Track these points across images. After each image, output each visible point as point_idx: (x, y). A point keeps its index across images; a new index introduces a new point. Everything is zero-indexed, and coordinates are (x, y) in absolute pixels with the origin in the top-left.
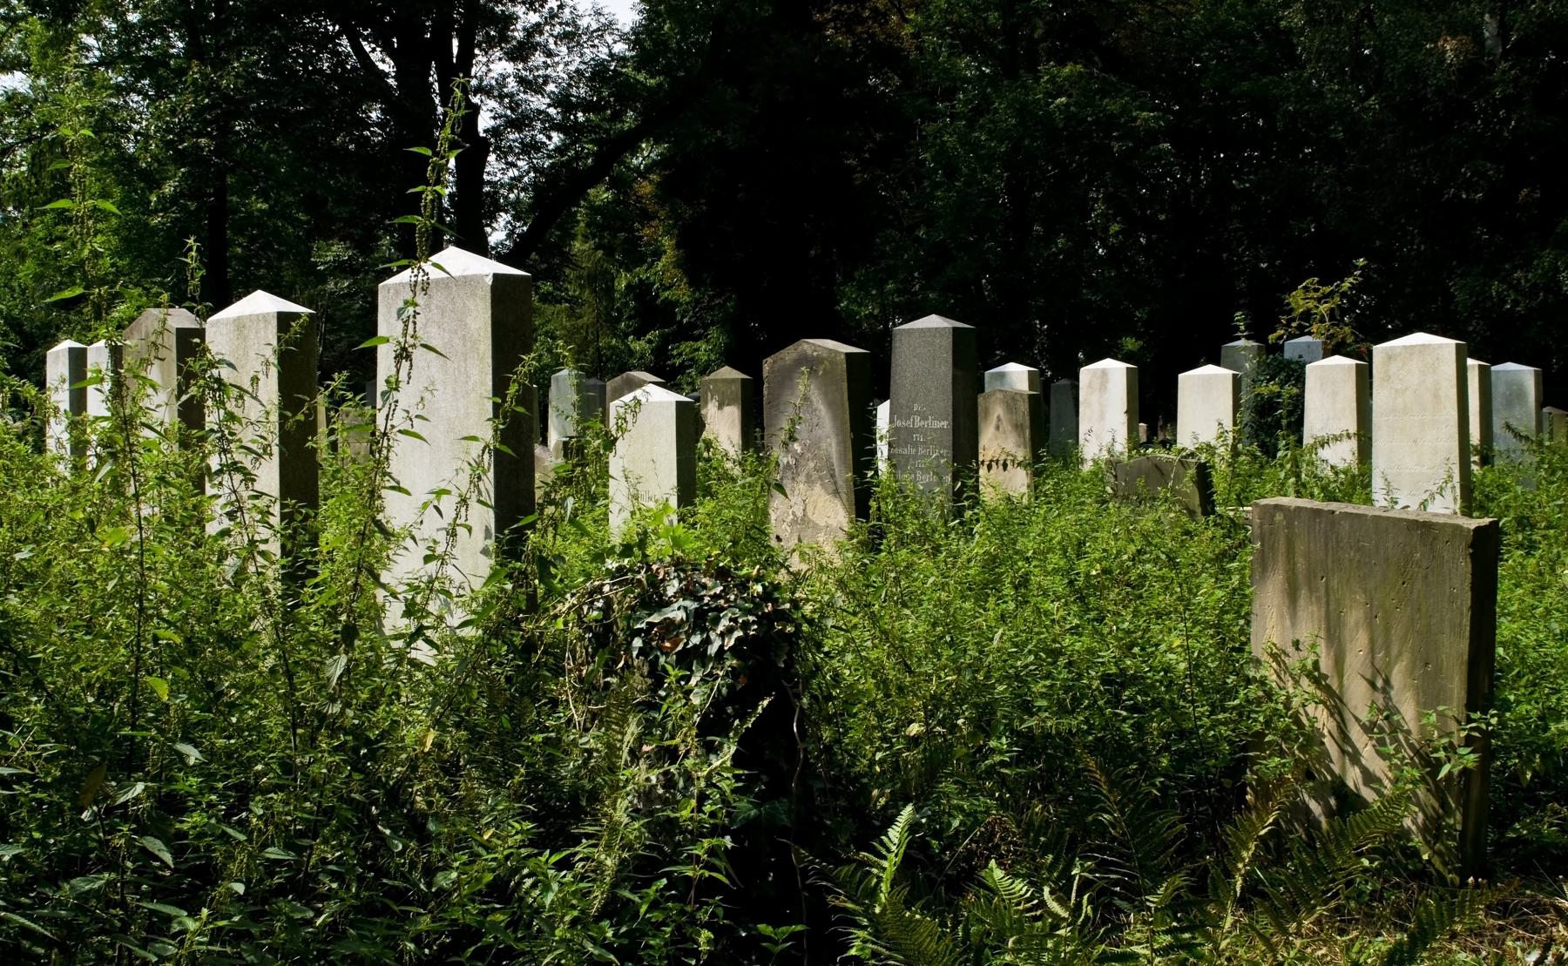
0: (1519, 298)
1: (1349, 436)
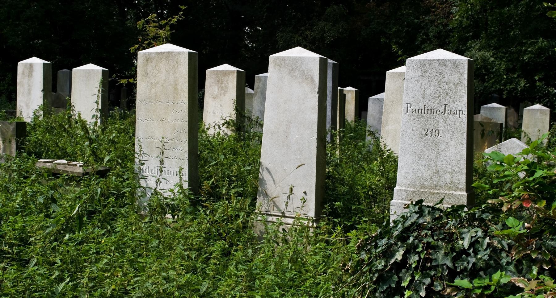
0: (308, 44)
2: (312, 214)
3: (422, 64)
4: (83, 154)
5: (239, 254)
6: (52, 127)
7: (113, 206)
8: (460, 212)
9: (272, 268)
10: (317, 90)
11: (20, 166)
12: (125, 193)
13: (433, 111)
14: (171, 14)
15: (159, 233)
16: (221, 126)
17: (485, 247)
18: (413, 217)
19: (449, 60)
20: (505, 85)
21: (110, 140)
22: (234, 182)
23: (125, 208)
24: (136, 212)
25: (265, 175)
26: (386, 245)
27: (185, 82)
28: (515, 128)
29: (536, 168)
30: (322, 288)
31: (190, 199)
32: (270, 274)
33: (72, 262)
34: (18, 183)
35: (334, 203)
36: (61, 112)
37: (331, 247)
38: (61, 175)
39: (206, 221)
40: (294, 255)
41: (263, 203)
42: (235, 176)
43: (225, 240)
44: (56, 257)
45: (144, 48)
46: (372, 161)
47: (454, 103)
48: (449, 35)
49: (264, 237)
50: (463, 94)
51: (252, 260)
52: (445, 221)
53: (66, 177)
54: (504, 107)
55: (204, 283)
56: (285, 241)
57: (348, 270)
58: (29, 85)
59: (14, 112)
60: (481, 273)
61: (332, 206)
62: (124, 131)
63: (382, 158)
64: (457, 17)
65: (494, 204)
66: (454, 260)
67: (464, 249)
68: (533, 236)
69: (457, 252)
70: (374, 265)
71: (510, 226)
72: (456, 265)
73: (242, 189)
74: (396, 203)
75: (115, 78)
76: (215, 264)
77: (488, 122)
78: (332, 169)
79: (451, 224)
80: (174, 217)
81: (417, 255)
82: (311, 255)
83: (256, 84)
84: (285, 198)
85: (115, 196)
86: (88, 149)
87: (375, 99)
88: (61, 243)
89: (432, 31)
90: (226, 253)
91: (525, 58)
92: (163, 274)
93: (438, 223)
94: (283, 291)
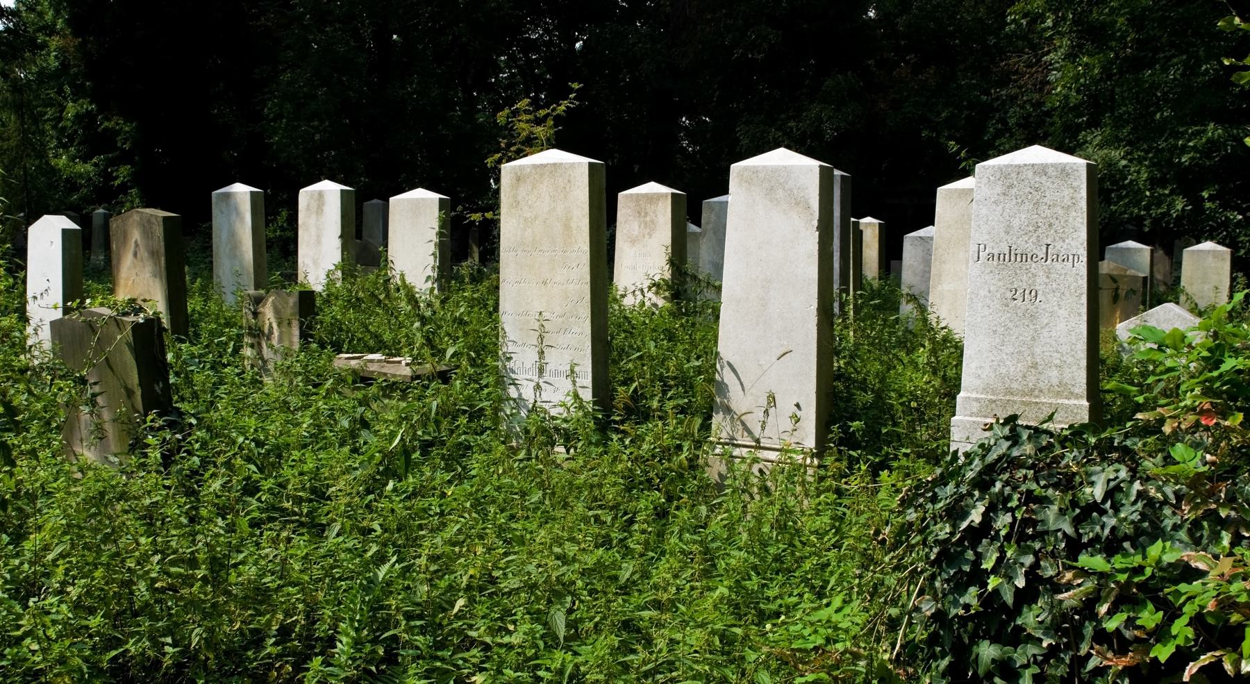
1: (56, 308)
2: (810, 443)
3: (1004, 173)
4: (410, 344)
5: (684, 514)
6: (358, 299)
7: (465, 433)
8: (1085, 436)
9: (744, 539)
10: (816, 223)
11: (307, 365)
12: (482, 409)
13: (1024, 257)
14: (555, 98)
15: (544, 477)
16: (646, 290)
17: (1133, 498)
18: (1000, 446)
19: (1052, 165)
20: (1147, 208)
21: (455, 320)
22: (671, 387)
23: (484, 436)
24: (503, 443)
25: (728, 377)
26: (952, 496)
27: (583, 216)
28: (1165, 284)
29: (1223, 356)
30: (832, 573)
31: (595, 418)
32: (740, 549)
33: (399, 530)
34: (304, 394)
35: (850, 424)
36: (372, 273)
37: (846, 502)
38: (375, 380)
39: (625, 457)
40: (781, 514)
41: (723, 424)
42: (675, 378)
43: (658, 490)
44: (372, 520)
45: (510, 160)
46: (914, 349)
47: (1064, 241)
48: (1044, 122)
49: (726, 483)
50: (1079, 225)
51: (705, 524)
52: (1058, 451)
53: (384, 384)
54: (1148, 248)
55: (624, 565)
56: (765, 490)
57: (884, 541)
58: (318, 228)
59: (293, 274)
60: (1126, 545)
61: (845, 429)
62: (479, 303)
63: (933, 343)
64: (1059, 89)
65: (1149, 421)
66: (1077, 522)
67: (1095, 501)
68: (1222, 479)
69: (1081, 508)
70: (931, 532)
71: (1178, 459)
72: (1081, 531)
73: (686, 400)
74: (961, 421)
75: (462, 212)
76: (643, 532)
77: (1121, 276)
78: (845, 364)
79: (1071, 458)
80: (568, 452)
81: (1009, 514)
82: (810, 515)
83: (704, 216)
84: (760, 414)
85: (467, 415)
86: (419, 335)
87: (916, 238)
88: (380, 495)
89: (1013, 115)
90: (661, 514)
91: (1183, 160)
92: (557, 550)
93: (1047, 457)
94: (764, 579)
